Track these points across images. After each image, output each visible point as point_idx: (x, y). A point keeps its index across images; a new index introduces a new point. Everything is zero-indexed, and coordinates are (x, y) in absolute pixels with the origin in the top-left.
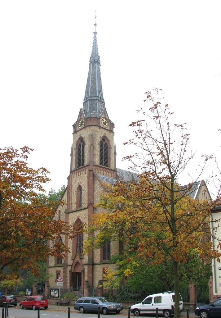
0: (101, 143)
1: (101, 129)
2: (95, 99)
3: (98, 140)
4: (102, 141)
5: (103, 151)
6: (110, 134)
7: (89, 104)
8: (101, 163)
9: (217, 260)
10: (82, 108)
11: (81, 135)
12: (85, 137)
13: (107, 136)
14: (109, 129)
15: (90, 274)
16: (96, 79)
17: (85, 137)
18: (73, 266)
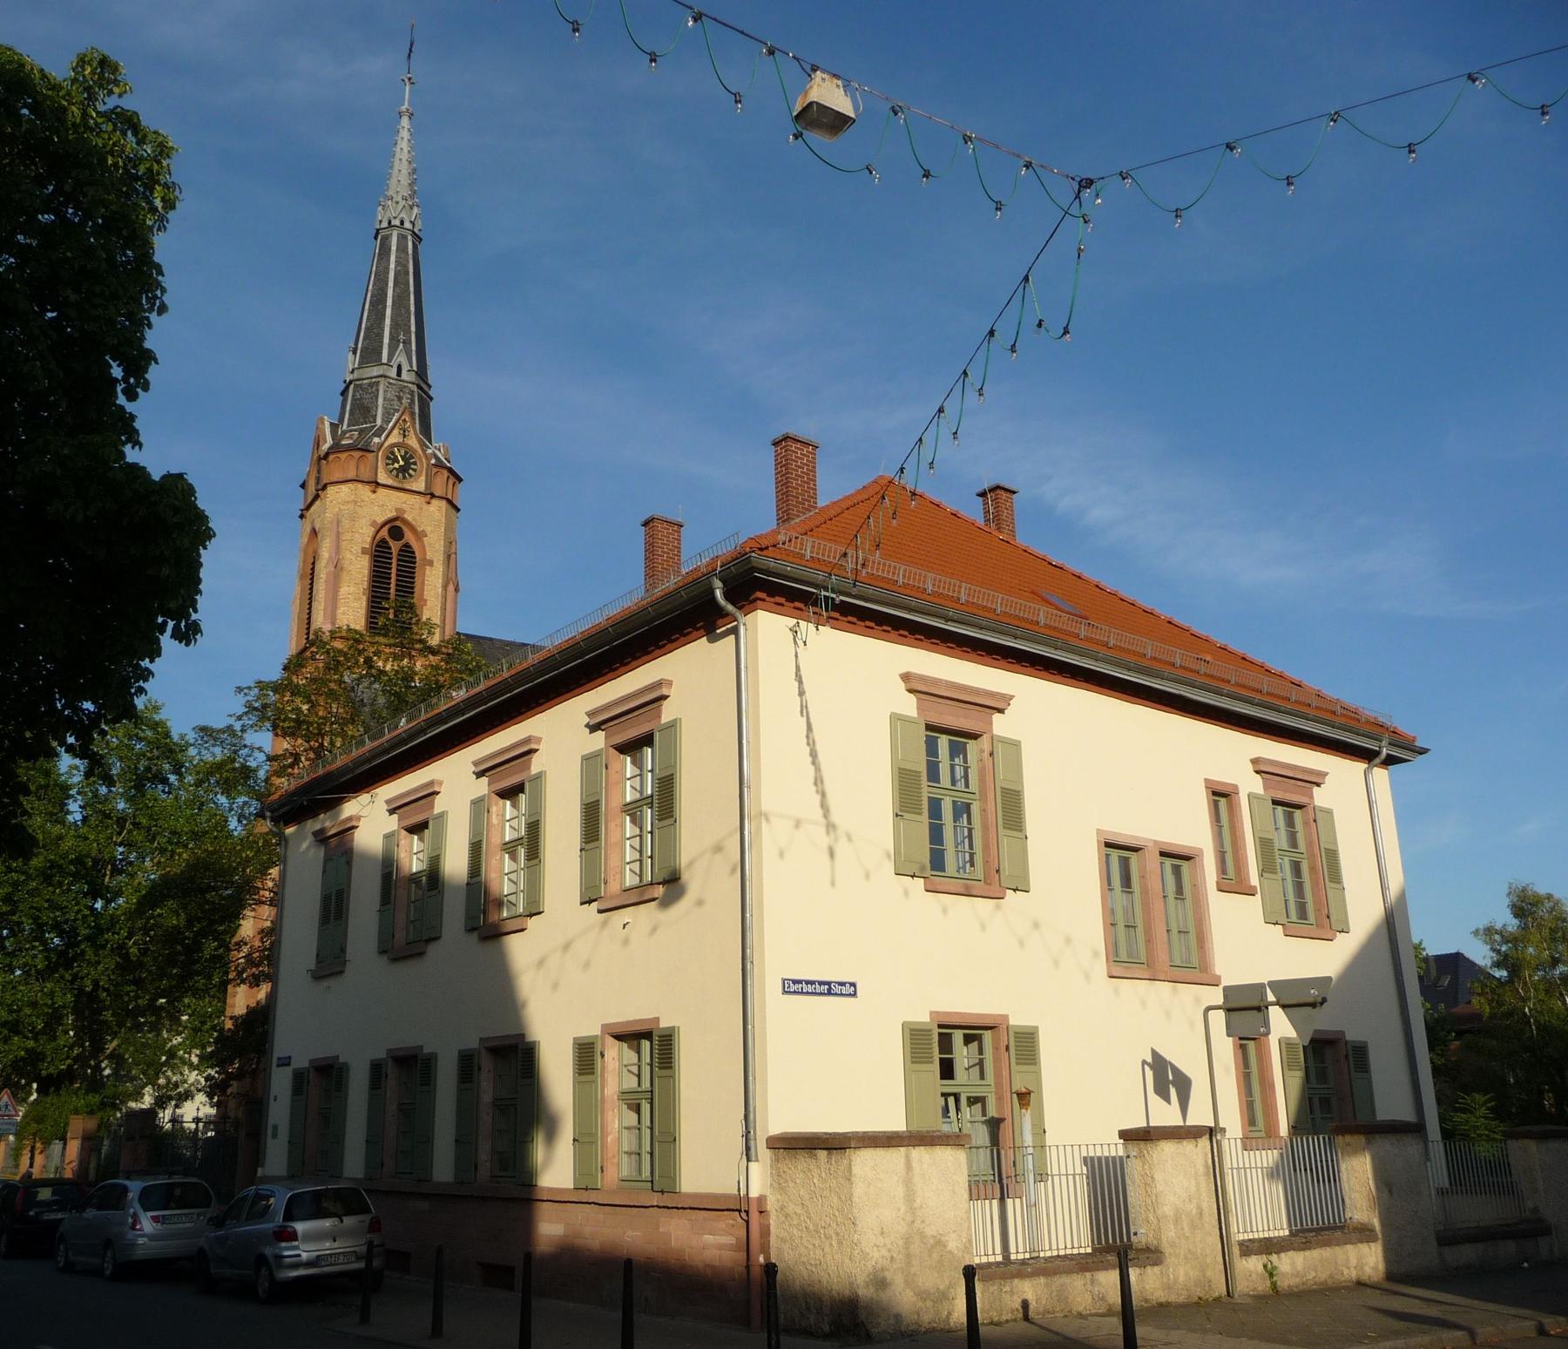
0: (379, 553)
3: (362, 536)
4: (388, 539)
6: (425, 506)
7: (353, 396)
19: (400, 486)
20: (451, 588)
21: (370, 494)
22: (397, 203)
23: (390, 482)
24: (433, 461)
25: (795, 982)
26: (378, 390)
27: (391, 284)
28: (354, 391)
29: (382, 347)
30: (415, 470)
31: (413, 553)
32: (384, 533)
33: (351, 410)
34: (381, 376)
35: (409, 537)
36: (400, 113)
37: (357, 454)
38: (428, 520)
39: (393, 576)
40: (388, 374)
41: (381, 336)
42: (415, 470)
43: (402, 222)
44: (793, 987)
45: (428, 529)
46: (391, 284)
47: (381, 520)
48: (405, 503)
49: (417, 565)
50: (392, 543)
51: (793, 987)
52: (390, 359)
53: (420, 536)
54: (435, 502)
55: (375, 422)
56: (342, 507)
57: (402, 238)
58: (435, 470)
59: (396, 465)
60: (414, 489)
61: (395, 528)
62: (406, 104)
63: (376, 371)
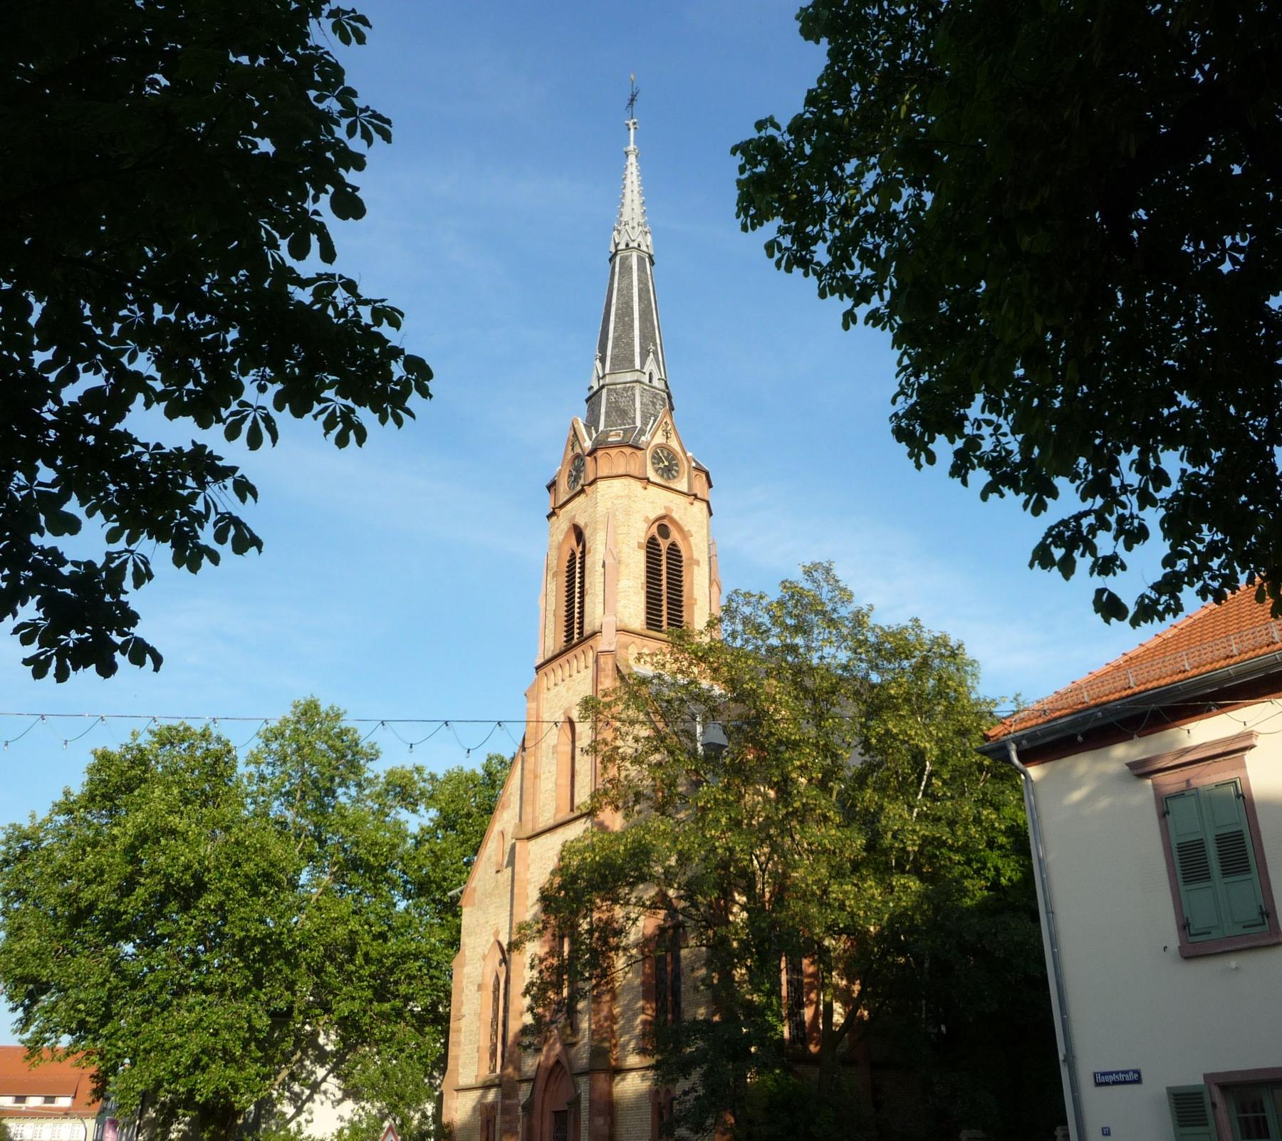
0: (652, 547)
1: (650, 487)
2: (629, 379)
3: (640, 532)
4: (657, 536)
5: (661, 575)
6: (689, 507)
7: (607, 399)
8: (653, 621)
9: (1168, 483)
10: (354, 100)
11: (574, 516)
12: (586, 525)
13: (676, 516)
14: (686, 490)
15: (600, 1121)
16: (632, 309)
17: (586, 525)
18: (540, 1084)
19: (667, 484)
20: (715, 589)
21: (642, 490)
22: (633, 228)
23: (658, 480)
24: (694, 464)
25: (1103, 1074)
26: (634, 395)
27: (636, 299)
28: (608, 395)
29: (633, 355)
30: (677, 471)
31: (679, 551)
32: (654, 529)
33: (607, 413)
34: (636, 381)
35: (675, 536)
36: (626, 153)
37: (628, 451)
38: (691, 517)
39: (664, 572)
40: (642, 380)
41: (631, 345)
42: (677, 471)
43: (639, 246)
44: (1103, 1080)
45: (693, 529)
46: (636, 299)
47: (653, 517)
48: (671, 502)
49: (683, 564)
50: (660, 540)
51: (1103, 1080)
52: (642, 366)
53: (685, 535)
54: (697, 503)
55: (634, 423)
56: (615, 501)
57: (641, 260)
58: (695, 473)
59: (661, 465)
60: (678, 489)
61: (663, 527)
62: (632, 143)
63: (629, 377)
